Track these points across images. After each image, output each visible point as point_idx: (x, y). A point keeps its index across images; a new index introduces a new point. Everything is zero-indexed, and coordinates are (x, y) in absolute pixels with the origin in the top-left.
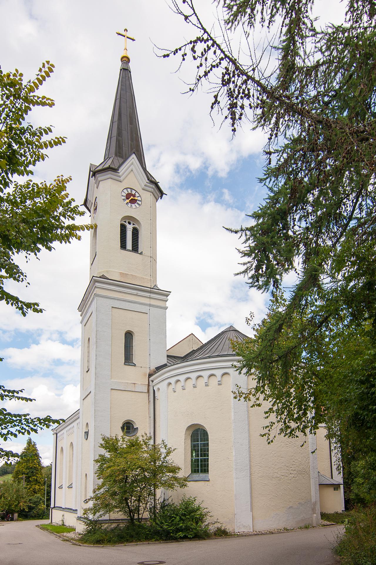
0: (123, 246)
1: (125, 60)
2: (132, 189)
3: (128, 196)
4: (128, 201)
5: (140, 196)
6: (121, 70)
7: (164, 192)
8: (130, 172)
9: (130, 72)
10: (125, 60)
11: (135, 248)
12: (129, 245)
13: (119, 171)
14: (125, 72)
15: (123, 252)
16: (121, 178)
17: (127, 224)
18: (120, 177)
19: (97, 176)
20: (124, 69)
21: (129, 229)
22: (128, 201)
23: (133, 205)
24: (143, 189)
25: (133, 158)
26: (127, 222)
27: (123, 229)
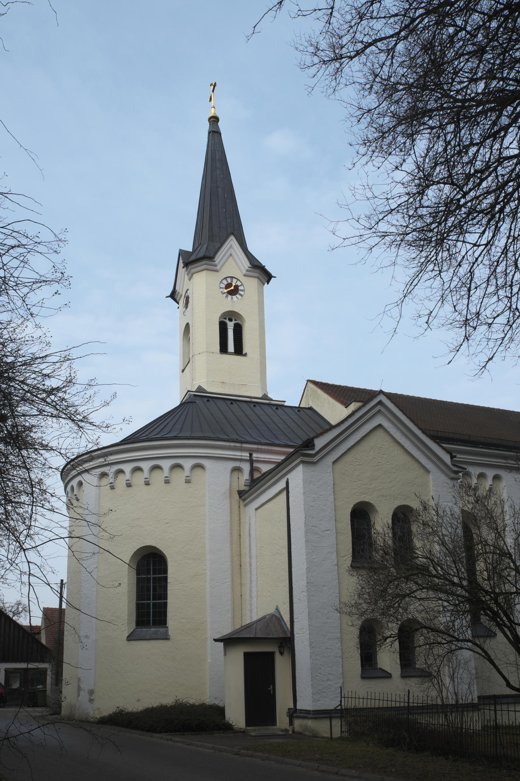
0: (224, 349)
1: (214, 120)
2: (232, 278)
3: (228, 286)
4: (226, 291)
5: (242, 285)
6: (209, 133)
7: (273, 275)
8: (231, 262)
9: (220, 134)
10: (214, 120)
11: (239, 350)
12: (231, 348)
13: (215, 259)
14: (215, 134)
15: (225, 357)
16: (218, 268)
17: (227, 321)
18: (216, 266)
19: (190, 267)
20: (213, 132)
21: (231, 326)
22: (226, 291)
23: (234, 297)
24: (245, 275)
25: (232, 241)
26: (227, 319)
27: (223, 327)
